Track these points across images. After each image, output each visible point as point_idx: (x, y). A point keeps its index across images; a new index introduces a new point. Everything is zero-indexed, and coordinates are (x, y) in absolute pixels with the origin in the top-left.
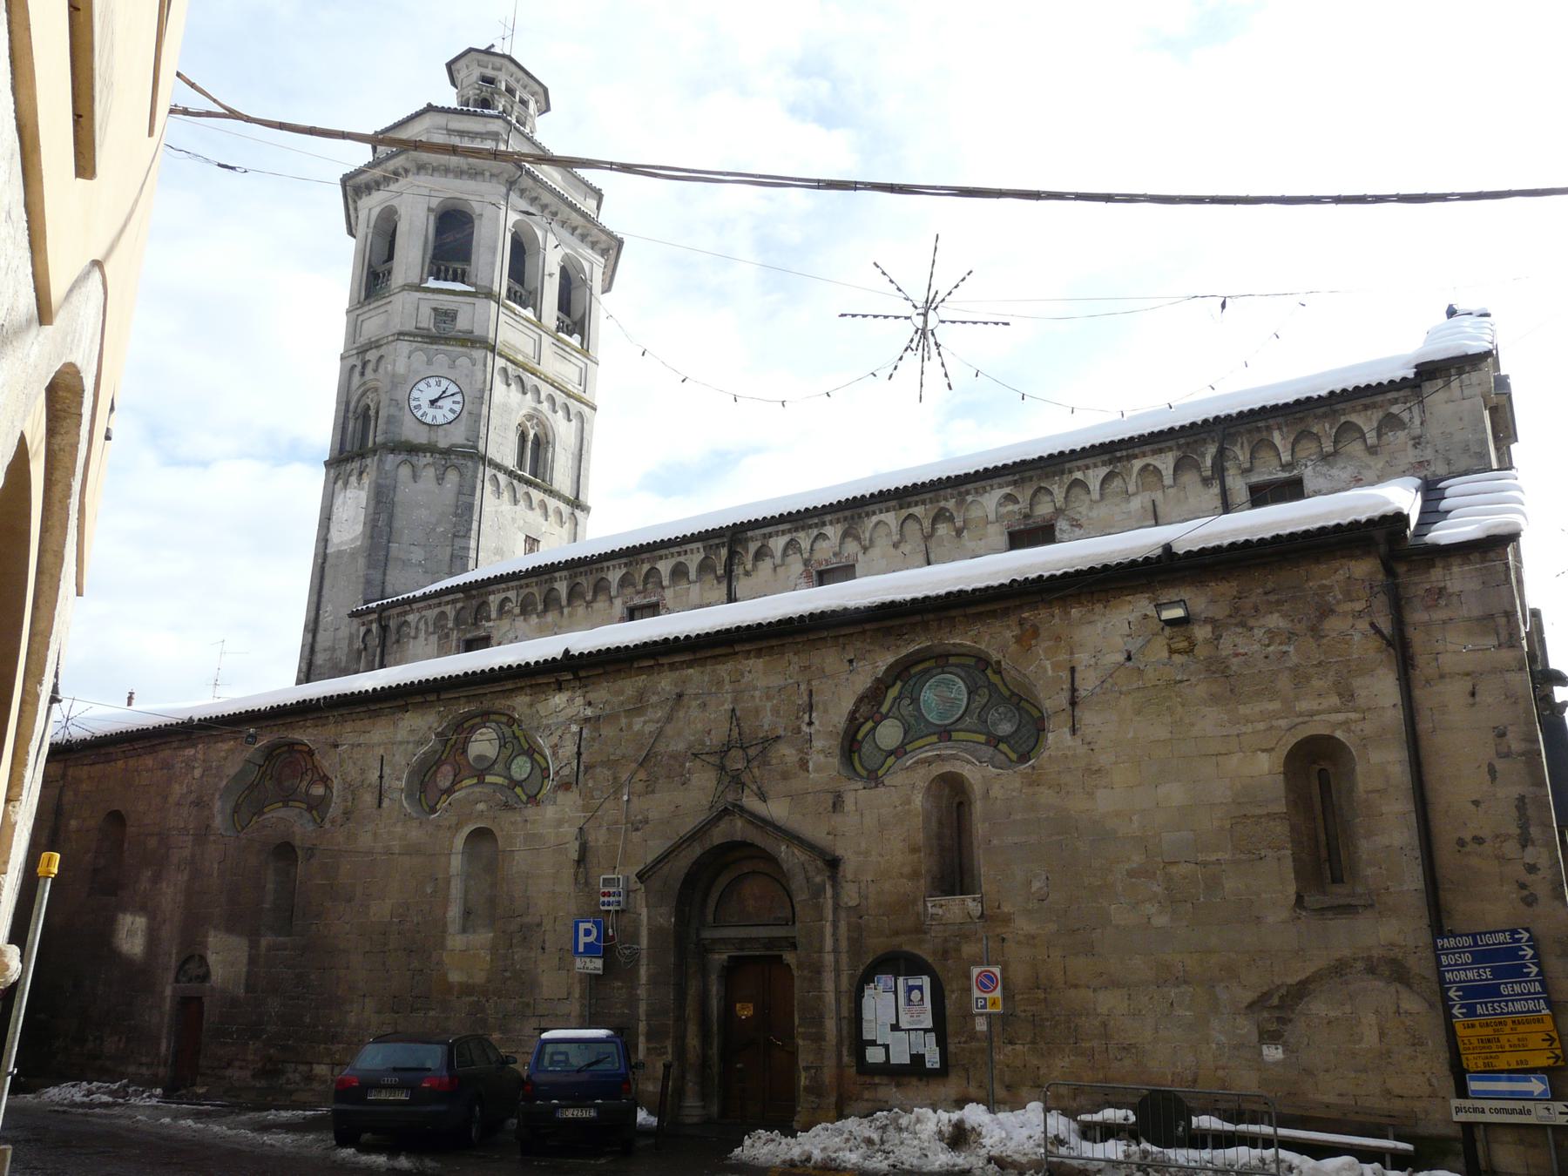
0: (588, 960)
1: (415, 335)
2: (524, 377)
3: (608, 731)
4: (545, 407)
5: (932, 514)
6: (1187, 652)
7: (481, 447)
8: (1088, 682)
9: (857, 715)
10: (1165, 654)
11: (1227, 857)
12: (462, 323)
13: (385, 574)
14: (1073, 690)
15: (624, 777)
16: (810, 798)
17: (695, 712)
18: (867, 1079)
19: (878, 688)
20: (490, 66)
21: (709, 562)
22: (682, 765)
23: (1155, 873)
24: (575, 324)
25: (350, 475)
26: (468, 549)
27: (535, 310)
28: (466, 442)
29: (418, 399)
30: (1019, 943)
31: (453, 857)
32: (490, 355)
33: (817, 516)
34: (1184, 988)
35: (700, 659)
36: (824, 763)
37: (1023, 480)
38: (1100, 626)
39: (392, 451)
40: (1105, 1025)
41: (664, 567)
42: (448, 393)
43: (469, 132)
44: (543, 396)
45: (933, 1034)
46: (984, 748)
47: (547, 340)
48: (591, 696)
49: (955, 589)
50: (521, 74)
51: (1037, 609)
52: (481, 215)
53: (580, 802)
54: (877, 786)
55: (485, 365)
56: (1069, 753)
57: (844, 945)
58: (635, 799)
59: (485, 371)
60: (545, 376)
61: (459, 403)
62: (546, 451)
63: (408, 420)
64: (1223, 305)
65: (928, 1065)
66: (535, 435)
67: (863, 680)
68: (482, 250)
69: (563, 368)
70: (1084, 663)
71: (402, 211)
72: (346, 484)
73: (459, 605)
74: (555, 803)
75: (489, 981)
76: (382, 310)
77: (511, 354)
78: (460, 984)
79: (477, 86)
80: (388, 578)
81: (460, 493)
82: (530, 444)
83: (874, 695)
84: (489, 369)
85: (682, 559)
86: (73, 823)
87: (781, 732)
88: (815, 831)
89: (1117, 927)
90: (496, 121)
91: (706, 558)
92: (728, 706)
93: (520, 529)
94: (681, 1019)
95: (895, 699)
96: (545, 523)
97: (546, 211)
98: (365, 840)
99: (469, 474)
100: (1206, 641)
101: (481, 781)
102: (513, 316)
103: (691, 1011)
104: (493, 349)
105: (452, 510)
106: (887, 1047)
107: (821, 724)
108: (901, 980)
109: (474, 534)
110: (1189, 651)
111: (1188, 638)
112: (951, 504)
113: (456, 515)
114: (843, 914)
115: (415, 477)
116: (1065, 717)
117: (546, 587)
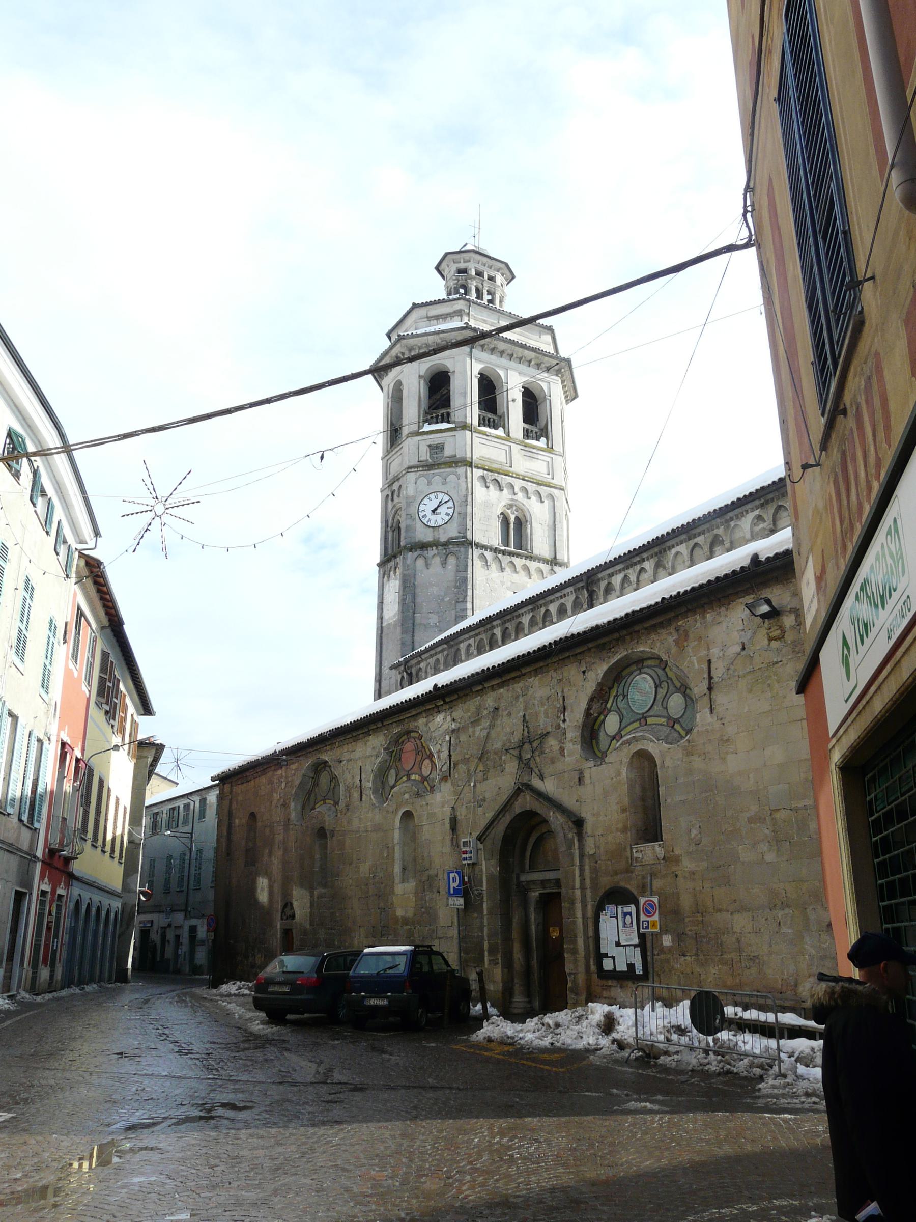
0: (455, 899)
1: (417, 467)
2: (499, 479)
3: (463, 738)
4: (520, 496)
5: (709, 540)
6: (780, 639)
7: (469, 536)
8: (718, 671)
9: (592, 712)
10: (766, 642)
11: (810, 803)
12: (448, 452)
13: (413, 636)
14: (710, 678)
15: (472, 769)
16: (566, 775)
17: (505, 719)
18: (604, 982)
19: (601, 690)
20: (462, 261)
21: (578, 600)
22: (501, 759)
23: (765, 819)
24: (542, 430)
25: (390, 571)
26: (466, 609)
27: (504, 428)
28: (458, 535)
29: (424, 511)
30: (685, 877)
31: (395, 831)
32: (469, 469)
33: (637, 555)
34: (787, 911)
35: (506, 681)
36: (573, 749)
37: (767, 502)
38: (724, 625)
39: (411, 550)
40: (738, 941)
41: (553, 608)
42: (443, 502)
43: (441, 315)
44: (517, 489)
45: (639, 949)
46: (665, 728)
47: (516, 448)
48: (455, 715)
49: (629, 610)
50: (485, 259)
51: (687, 617)
52: (454, 372)
53: (452, 789)
54: (601, 764)
55: (466, 477)
56: (710, 728)
57: (588, 882)
58: (478, 785)
59: (466, 482)
60: (516, 474)
61: (451, 508)
62: (526, 528)
63: (419, 527)
64: (322, 458)
65: (637, 972)
66: (517, 518)
67: (590, 687)
68: (457, 396)
69: (537, 466)
70: (716, 657)
71: (404, 383)
72: (389, 577)
73: (445, 653)
74: (440, 791)
75: (415, 915)
76: (399, 453)
77: (487, 465)
78: (402, 917)
79: (454, 278)
80: (415, 638)
81: (458, 571)
82: (512, 526)
83: (601, 695)
84: (469, 480)
85: (562, 601)
86: (237, 821)
87: (550, 729)
88: (568, 799)
89: (743, 863)
90: (459, 301)
91: (577, 598)
92: (521, 714)
93: (508, 588)
94: (507, 939)
95: (615, 697)
96: (529, 580)
97: (504, 355)
98: (356, 823)
99: (462, 557)
100: (792, 627)
101: (409, 779)
102: (485, 437)
103: (515, 934)
104: (470, 465)
105: (453, 584)
106: (613, 958)
107: (570, 721)
108: (620, 907)
109: (469, 599)
110: (780, 638)
111: (781, 627)
112: (720, 531)
113: (456, 587)
114: (587, 860)
115: (427, 565)
116: (706, 698)
117: (489, 633)
